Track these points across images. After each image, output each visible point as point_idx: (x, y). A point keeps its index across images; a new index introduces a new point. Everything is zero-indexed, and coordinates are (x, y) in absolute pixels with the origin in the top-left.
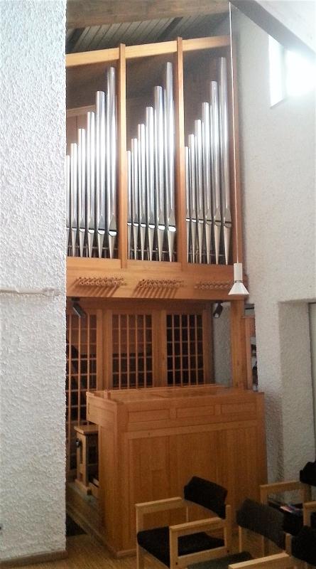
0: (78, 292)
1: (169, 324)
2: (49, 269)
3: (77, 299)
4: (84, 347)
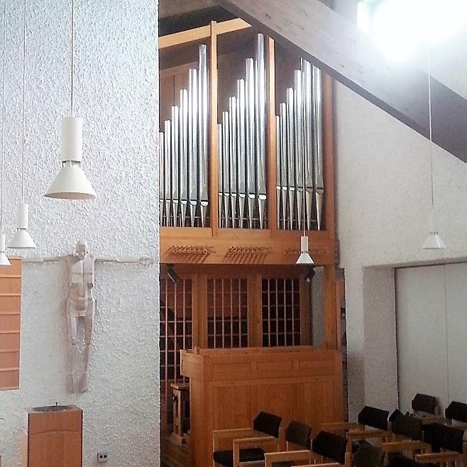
0: (172, 259)
1: (265, 288)
2: (144, 240)
3: (172, 265)
4: (180, 310)
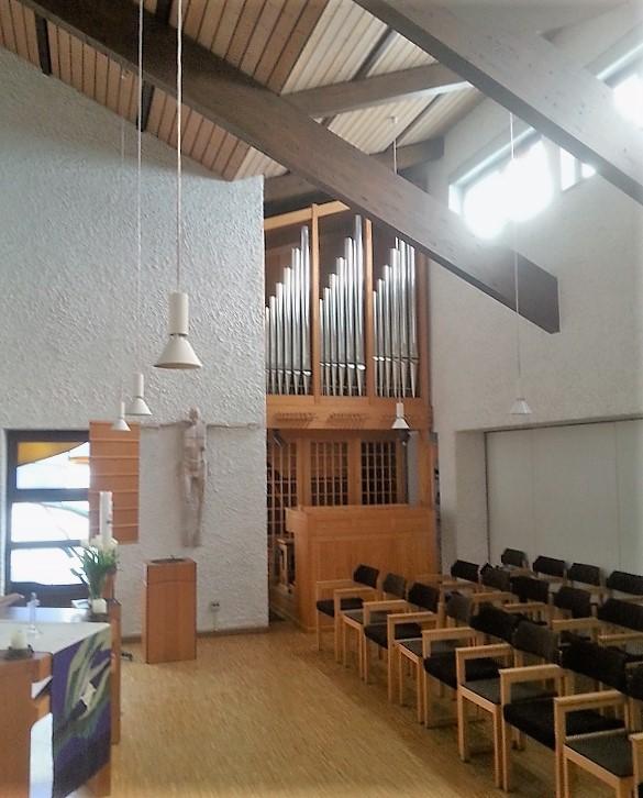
1: (364, 451)
3: (276, 430)
4: (285, 472)
